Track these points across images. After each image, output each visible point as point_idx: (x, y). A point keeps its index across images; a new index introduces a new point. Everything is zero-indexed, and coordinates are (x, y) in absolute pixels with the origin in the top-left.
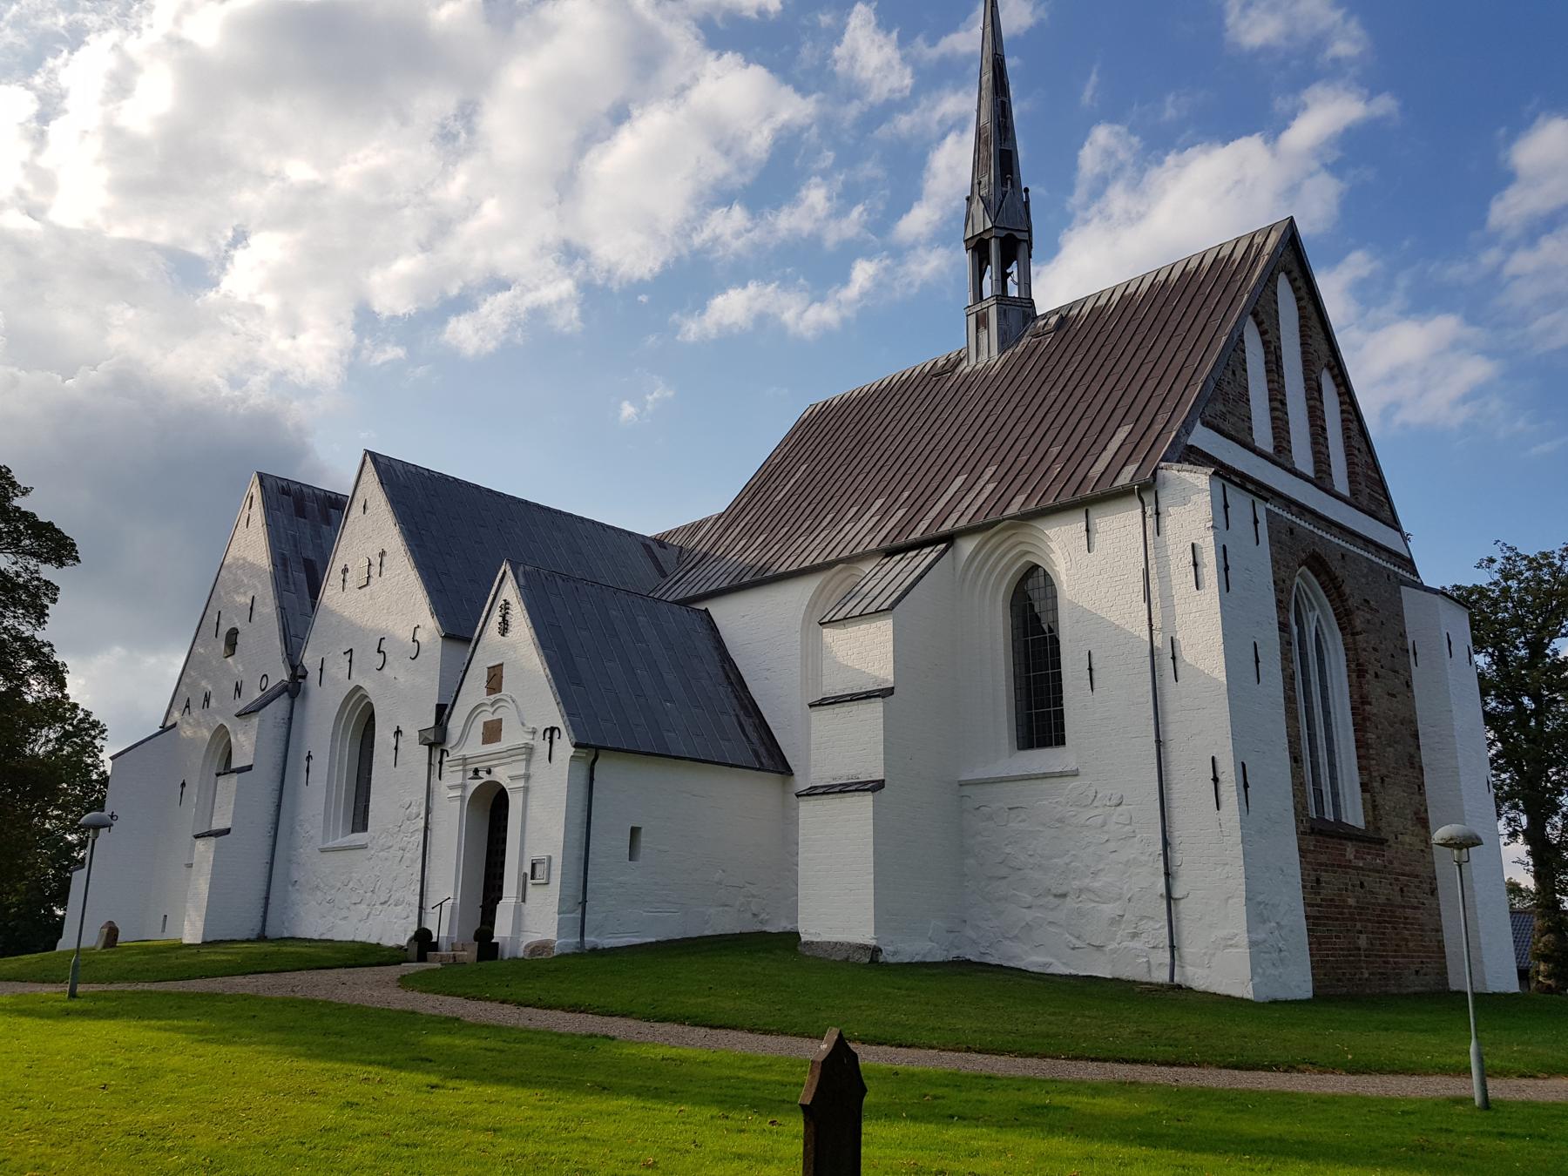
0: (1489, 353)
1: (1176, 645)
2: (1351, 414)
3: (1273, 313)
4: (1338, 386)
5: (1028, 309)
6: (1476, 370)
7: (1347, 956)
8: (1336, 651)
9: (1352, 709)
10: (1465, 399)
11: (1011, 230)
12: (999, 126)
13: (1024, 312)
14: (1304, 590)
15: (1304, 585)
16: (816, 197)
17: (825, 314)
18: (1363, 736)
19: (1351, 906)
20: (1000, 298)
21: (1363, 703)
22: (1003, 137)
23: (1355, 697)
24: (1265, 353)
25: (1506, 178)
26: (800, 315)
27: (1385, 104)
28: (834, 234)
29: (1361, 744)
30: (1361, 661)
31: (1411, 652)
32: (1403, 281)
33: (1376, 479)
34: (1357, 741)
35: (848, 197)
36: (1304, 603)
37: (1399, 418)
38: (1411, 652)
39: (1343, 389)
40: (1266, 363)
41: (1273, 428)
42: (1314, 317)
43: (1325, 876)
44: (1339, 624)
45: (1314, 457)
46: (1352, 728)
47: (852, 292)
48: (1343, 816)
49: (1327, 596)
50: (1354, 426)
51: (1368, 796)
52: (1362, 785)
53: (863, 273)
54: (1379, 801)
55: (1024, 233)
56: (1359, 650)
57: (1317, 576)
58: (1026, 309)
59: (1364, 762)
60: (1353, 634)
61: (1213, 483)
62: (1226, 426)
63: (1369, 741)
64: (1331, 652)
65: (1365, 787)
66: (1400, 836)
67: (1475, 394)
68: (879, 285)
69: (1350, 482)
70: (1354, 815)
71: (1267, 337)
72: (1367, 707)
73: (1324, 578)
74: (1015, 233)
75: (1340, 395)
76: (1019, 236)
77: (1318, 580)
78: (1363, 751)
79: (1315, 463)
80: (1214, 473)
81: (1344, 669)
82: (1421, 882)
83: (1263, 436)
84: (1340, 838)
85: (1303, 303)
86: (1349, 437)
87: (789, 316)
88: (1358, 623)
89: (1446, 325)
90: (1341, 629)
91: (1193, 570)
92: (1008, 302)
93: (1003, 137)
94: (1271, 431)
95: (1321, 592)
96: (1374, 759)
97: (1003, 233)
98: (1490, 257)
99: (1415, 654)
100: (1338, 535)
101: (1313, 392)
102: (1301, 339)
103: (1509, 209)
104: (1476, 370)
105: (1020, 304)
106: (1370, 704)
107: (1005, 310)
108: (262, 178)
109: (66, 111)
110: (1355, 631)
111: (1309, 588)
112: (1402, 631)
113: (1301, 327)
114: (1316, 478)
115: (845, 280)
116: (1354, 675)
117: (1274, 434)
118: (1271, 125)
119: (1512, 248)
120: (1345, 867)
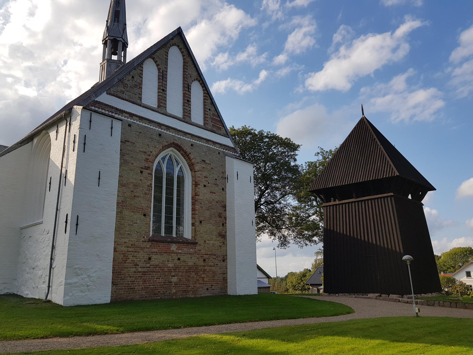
0: (444, 100)
1: (67, 171)
2: (207, 97)
3: (164, 59)
4: (203, 87)
5: (119, 64)
6: (440, 104)
7: (163, 285)
8: (188, 178)
9: (192, 197)
10: (435, 113)
11: (115, 37)
12: (116, 2)
13: (117, 65)
14: (173, 155)
15: (174, 154)
16: (251, 49)
17: (248, 87)
18: (194, 207)
19: (169, 267)
20: (108, 60)
21: (196, 195)
22: (117, 6)
23: (193, 193)
24: (159, 73)
25: (456, 44)
26: (240, 89)
27: (427, 23)
28: (254, 62)
29: (193, 210)
30: (196, 181)
31: (227, 178)
32: (422, 77)
33: (219, 120)
34: (192, 208)
35: (260, 52)
36: (174, 161)
37: (415, 119)
38: (227, 178)
39: (204, 88)
40: (158, 76)
41: (158, 99)
42: (190, 62)
43: (154, 257)
44: (190, 168)
45: (183, 111)
46: (191, 204)
47: (258, 82)
48: (184, 235)
49: (185, 159)
50: (209, 101)
51: (194, 227)
52: (192, 224)
53: (263, 74)
54: (197, 229)
55: (120, 38)
56: (196, 177)
57: (179, 152)
58: (118, 64)
59: (193, 216)
60: (195, 172)
61: (83, 111)
62: (124, 96)
63: (196, 209)
64: (187, 178)
65: (193, 225)
66: (207, 241)
67: (438, 112)
68: (267, 78)
69: (204, 120)
70: (188, 233)
71: (159, 67)
72: (197, 197)
73: (182, 152)
74: (117, 38)
75: (203, 90)
76: (118, 39)
77: (180, 153)
78: (193, 212)
79: (183, 112)
80: (83, 108)
81: (191, 184)
82: (217, 257)
83: (154, 103)
84: (168, 243)
85: (185, 57)
86: (205, 105)
87: (237, 88)
88: (197, 168)
89: (432, 91)
90: (191, 170)
91: (73, 144)
92: (111, 61)
93: (117, 6)
94: (157, 100)
95: (182, 157)
96: (197, 215)
97: (112, 38)
98: (449, 69)
99: (227, 179)
100: (191, 138)
101: (187, 89)
102: (183, 70)
103: (457, 55)
104: (440, 104)
105: (116, 62)
106: (198, 195)
107: (110, 64)
108: (75, 44)
109: (10, 22)
110: (195, 171)
111: (176, 154)
112: (223, 171)
113: (184, 65)
114: (183, 118)
115: (257, 77)
116: (194, 186)
117: (158, 101)
118: (393, 29)
119: (455, 67)
120: (169, 253)
